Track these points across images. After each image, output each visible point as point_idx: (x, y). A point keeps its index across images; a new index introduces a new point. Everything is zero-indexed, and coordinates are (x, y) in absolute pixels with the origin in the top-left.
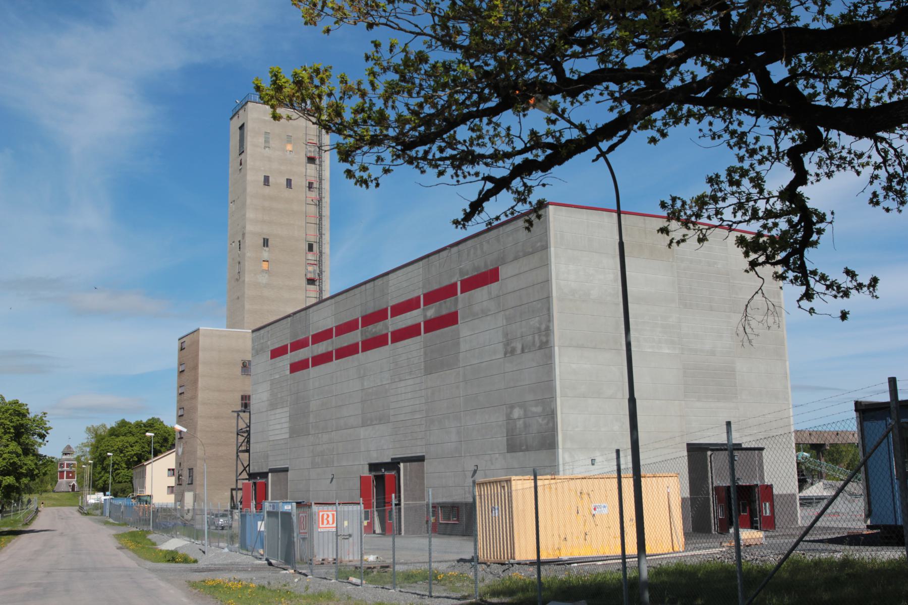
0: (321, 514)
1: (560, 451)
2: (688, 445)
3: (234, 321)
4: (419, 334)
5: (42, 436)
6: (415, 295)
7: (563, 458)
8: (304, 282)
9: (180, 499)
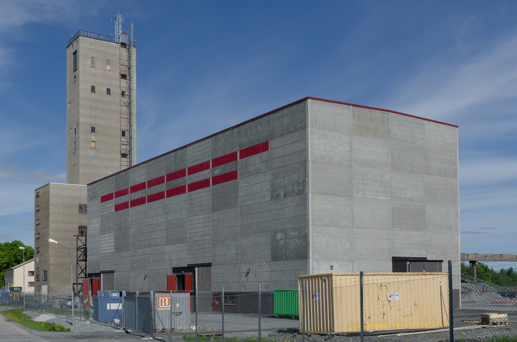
0: (160, 299)
1: (311, 260)
2: (393, 258)
3: (73, 178)
4: (209, 185)
7: (312, 265)
8: (119, 156)
9: (38, 289)
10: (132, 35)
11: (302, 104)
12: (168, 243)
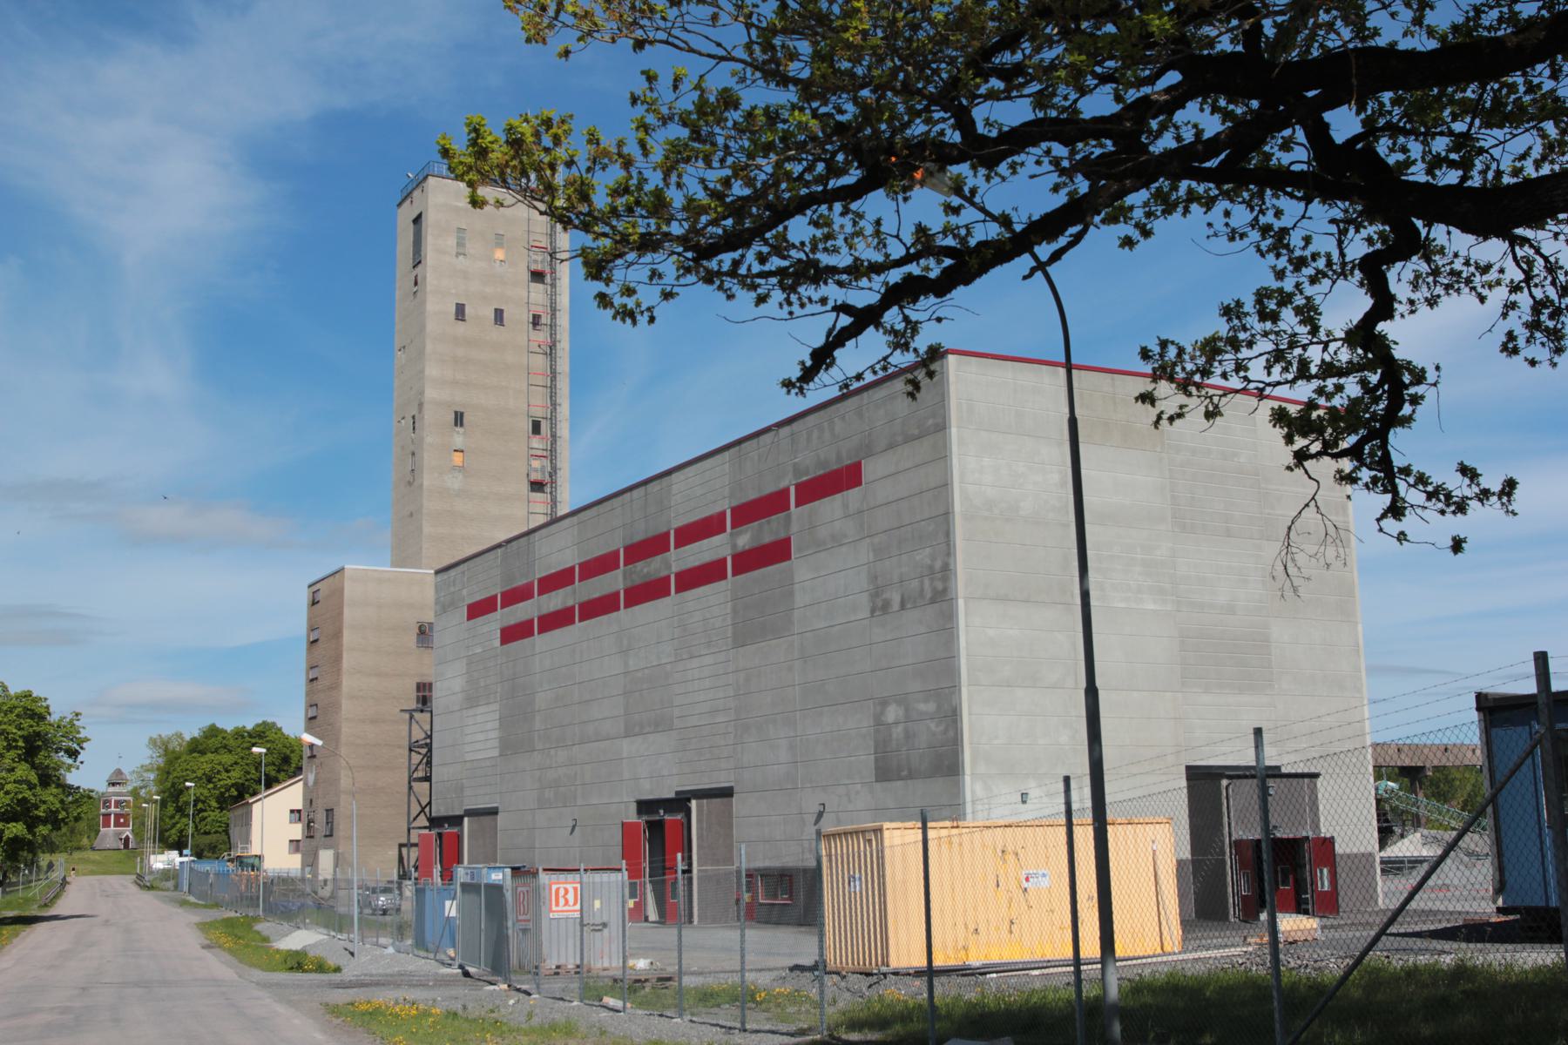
0: (554, 887)
1: (968, 779)
2: (1188, 768)
3: (404, 554)
4: (724, 577)
5: (73, 754)
6: (717, 509)
7: (973, 792)
8: (525, 487)
9: (311, 861)
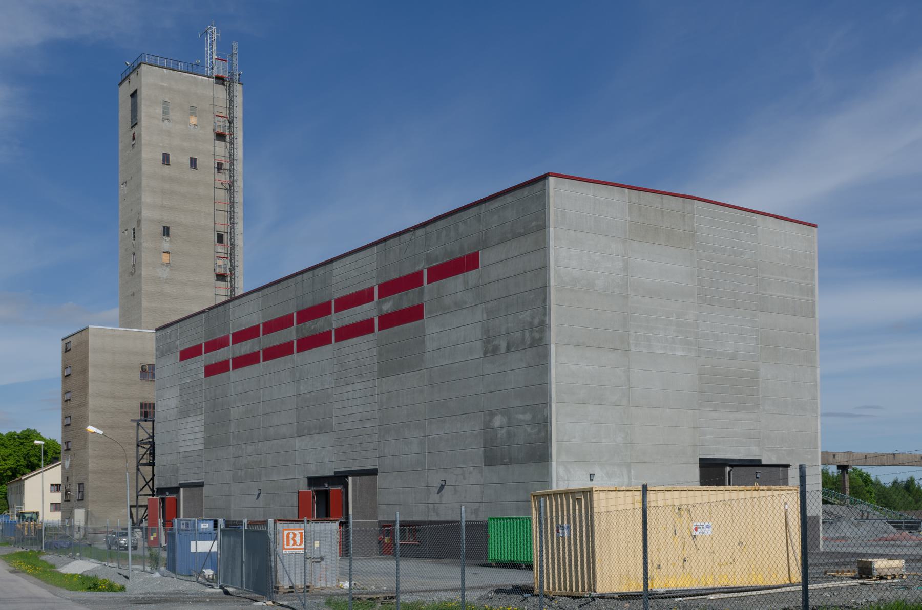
0: (286, 533)
1: (554, 464)
2: (701, 459)
3: (130, 317)
4: (372, 331)
7: (557, 473)
8: (212, 278)
9: (68, 516)
10: (235, 62)
11: (539, 186)
12: (300, 434)
